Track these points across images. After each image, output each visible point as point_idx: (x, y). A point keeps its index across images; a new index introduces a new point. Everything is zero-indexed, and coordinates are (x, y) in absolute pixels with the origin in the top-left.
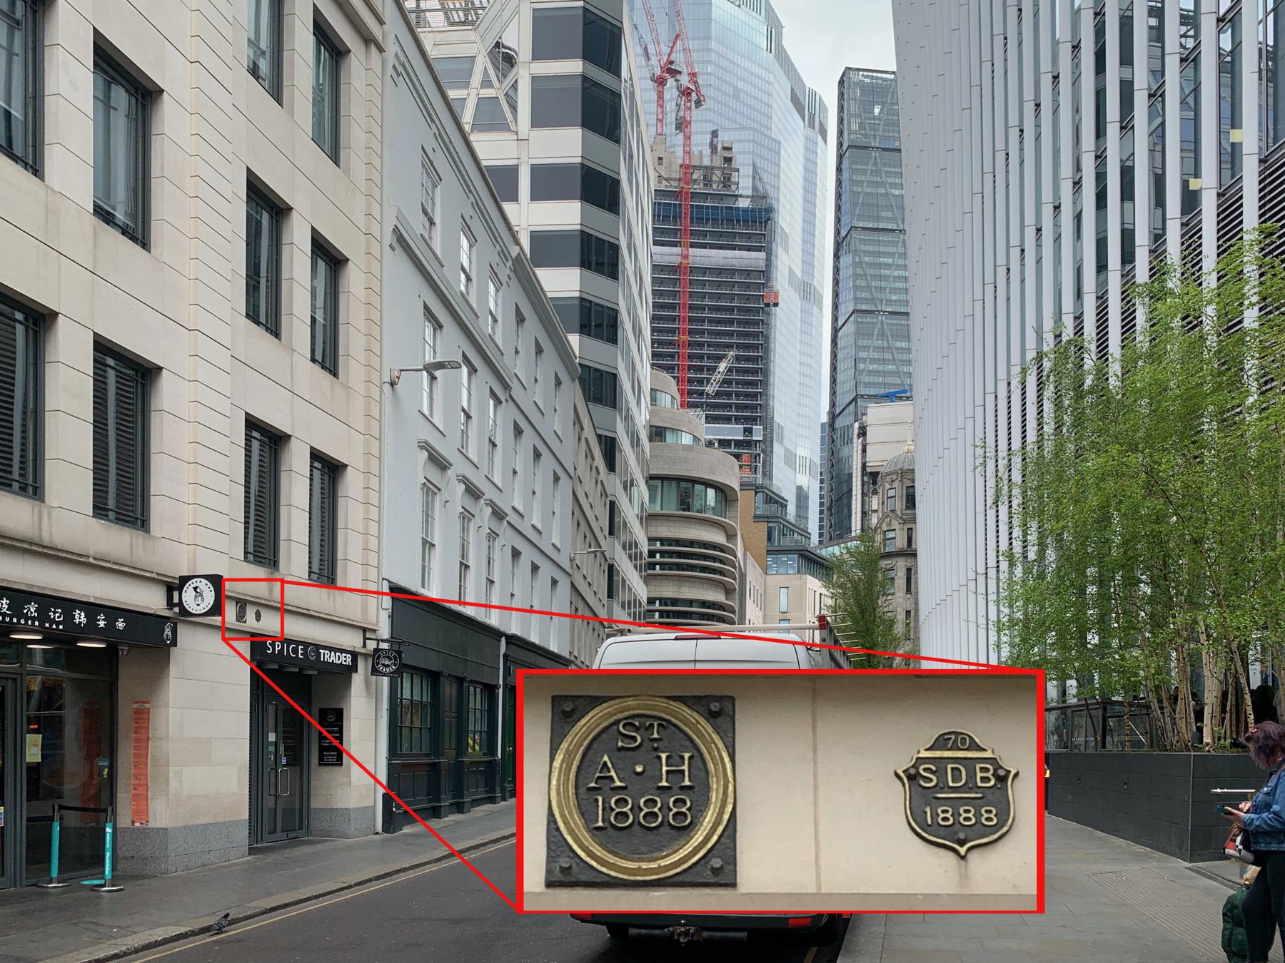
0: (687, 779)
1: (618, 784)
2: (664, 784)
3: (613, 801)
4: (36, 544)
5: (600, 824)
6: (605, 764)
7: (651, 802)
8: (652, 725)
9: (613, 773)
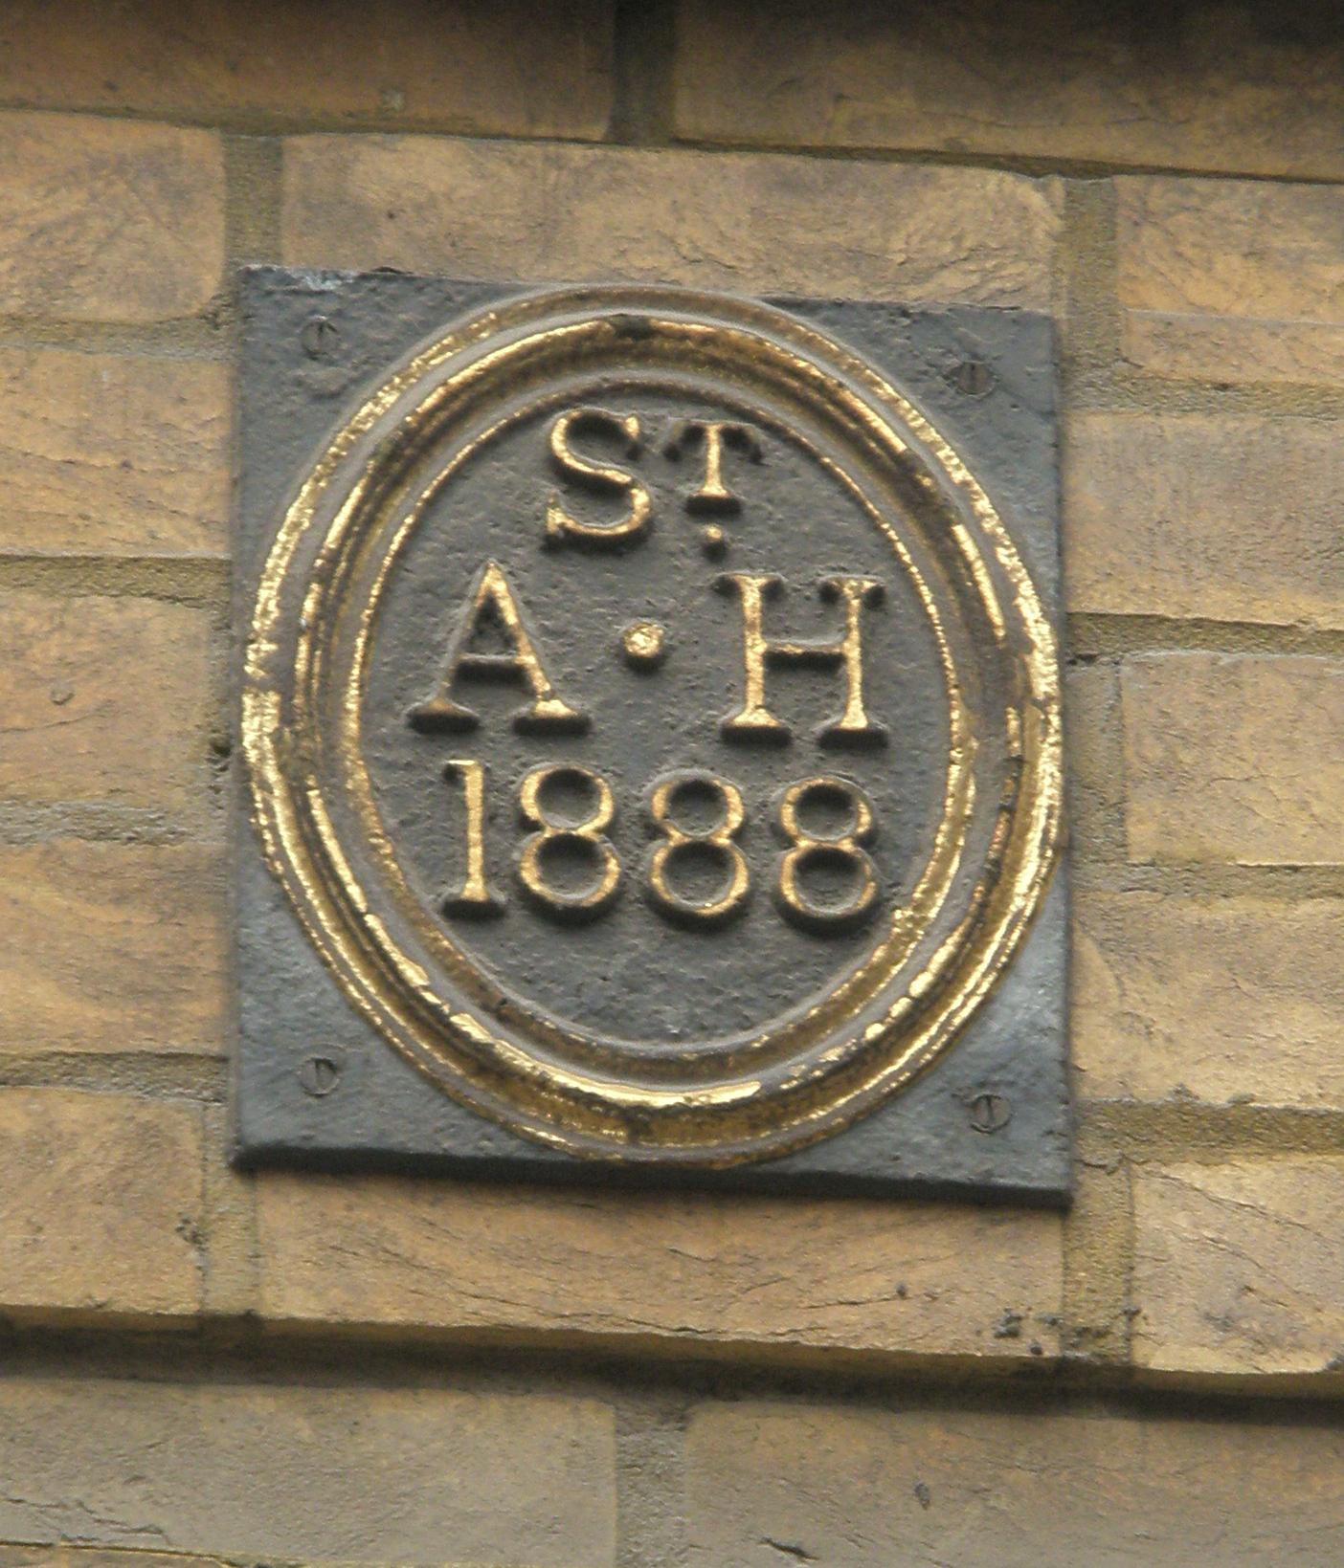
0: (856, 705)
1: (556, 708)
2: (753, 715)
3: (531, 785)
4: (928, 156)
5: (474, 888)
6: (489, 613)
7: (697, 797)
8: (694, 436)
9: (528, 659)
